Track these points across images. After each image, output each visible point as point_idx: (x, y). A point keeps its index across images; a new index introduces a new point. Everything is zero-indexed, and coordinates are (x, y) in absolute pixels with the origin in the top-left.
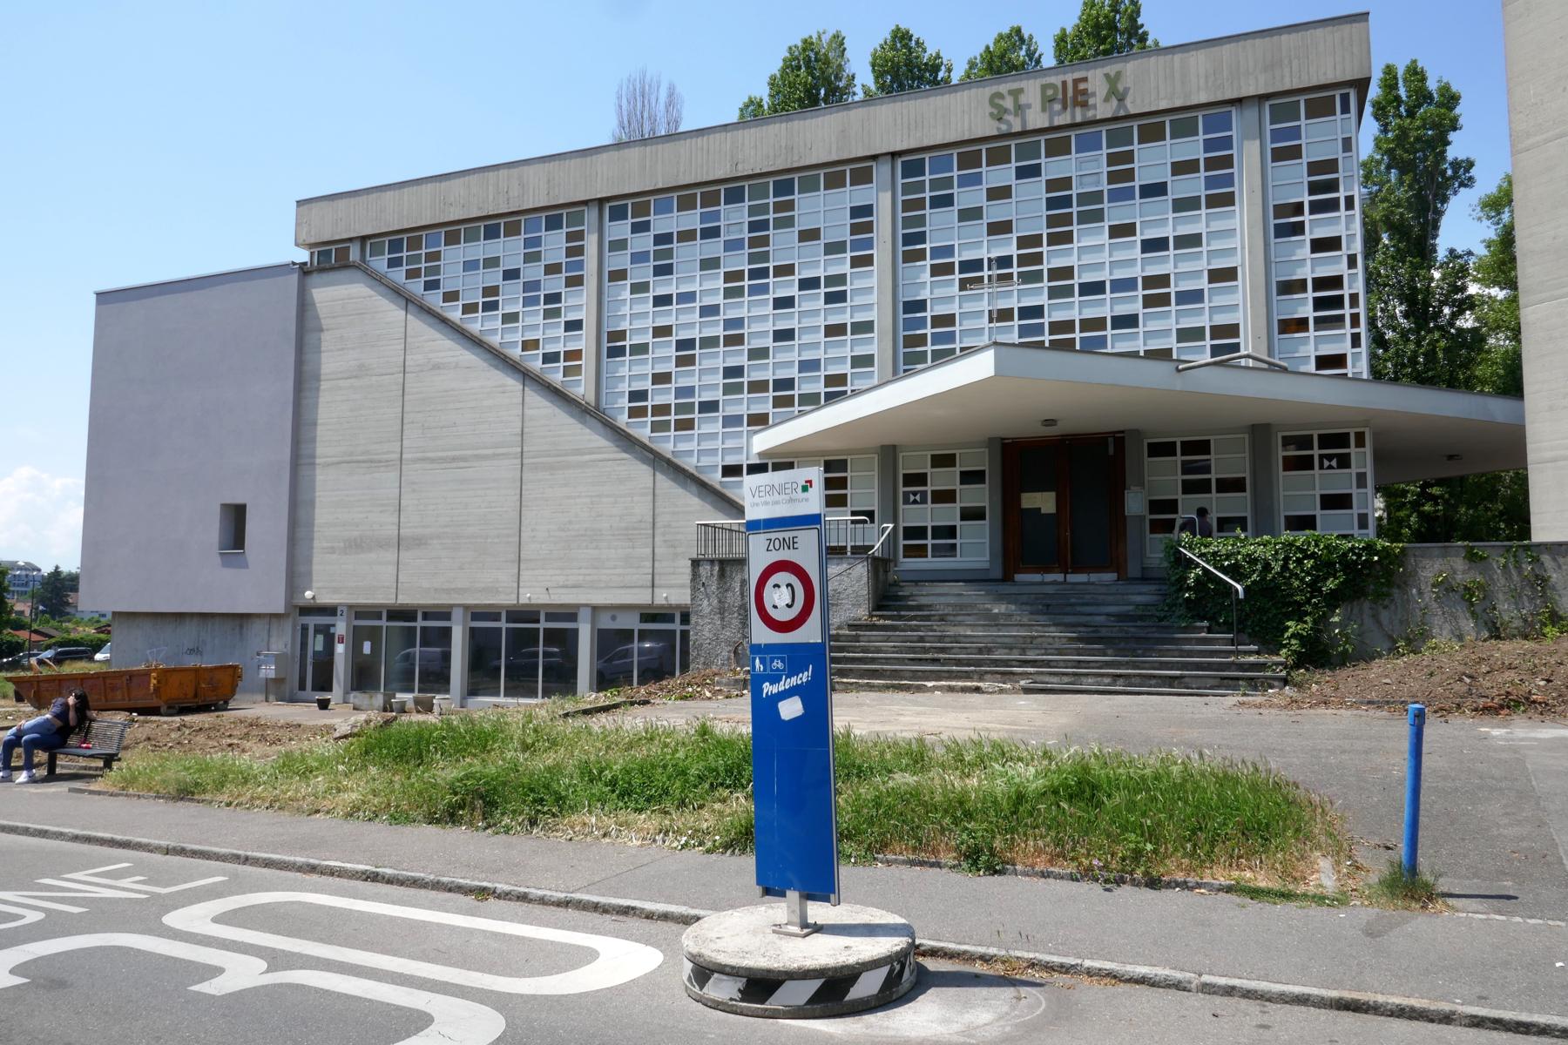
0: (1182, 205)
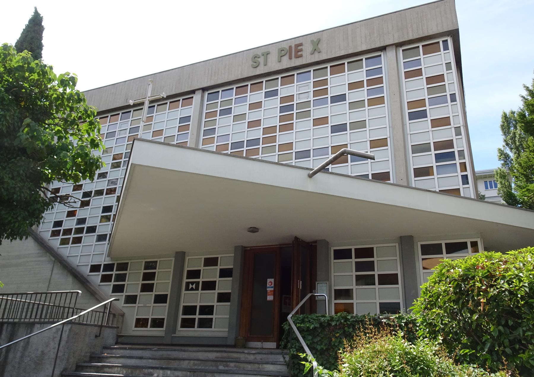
0: (353, 105)
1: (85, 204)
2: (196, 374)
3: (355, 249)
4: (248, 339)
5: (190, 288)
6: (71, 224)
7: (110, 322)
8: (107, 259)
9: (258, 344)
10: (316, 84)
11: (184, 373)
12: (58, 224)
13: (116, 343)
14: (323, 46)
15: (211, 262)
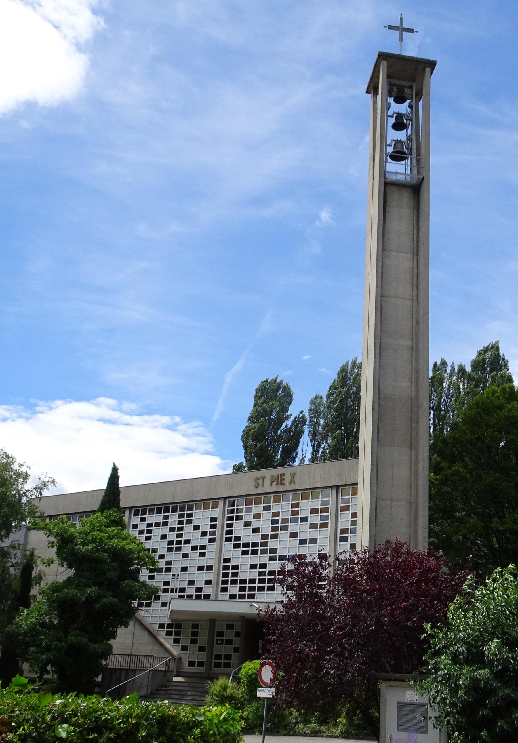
0: (313, 526)
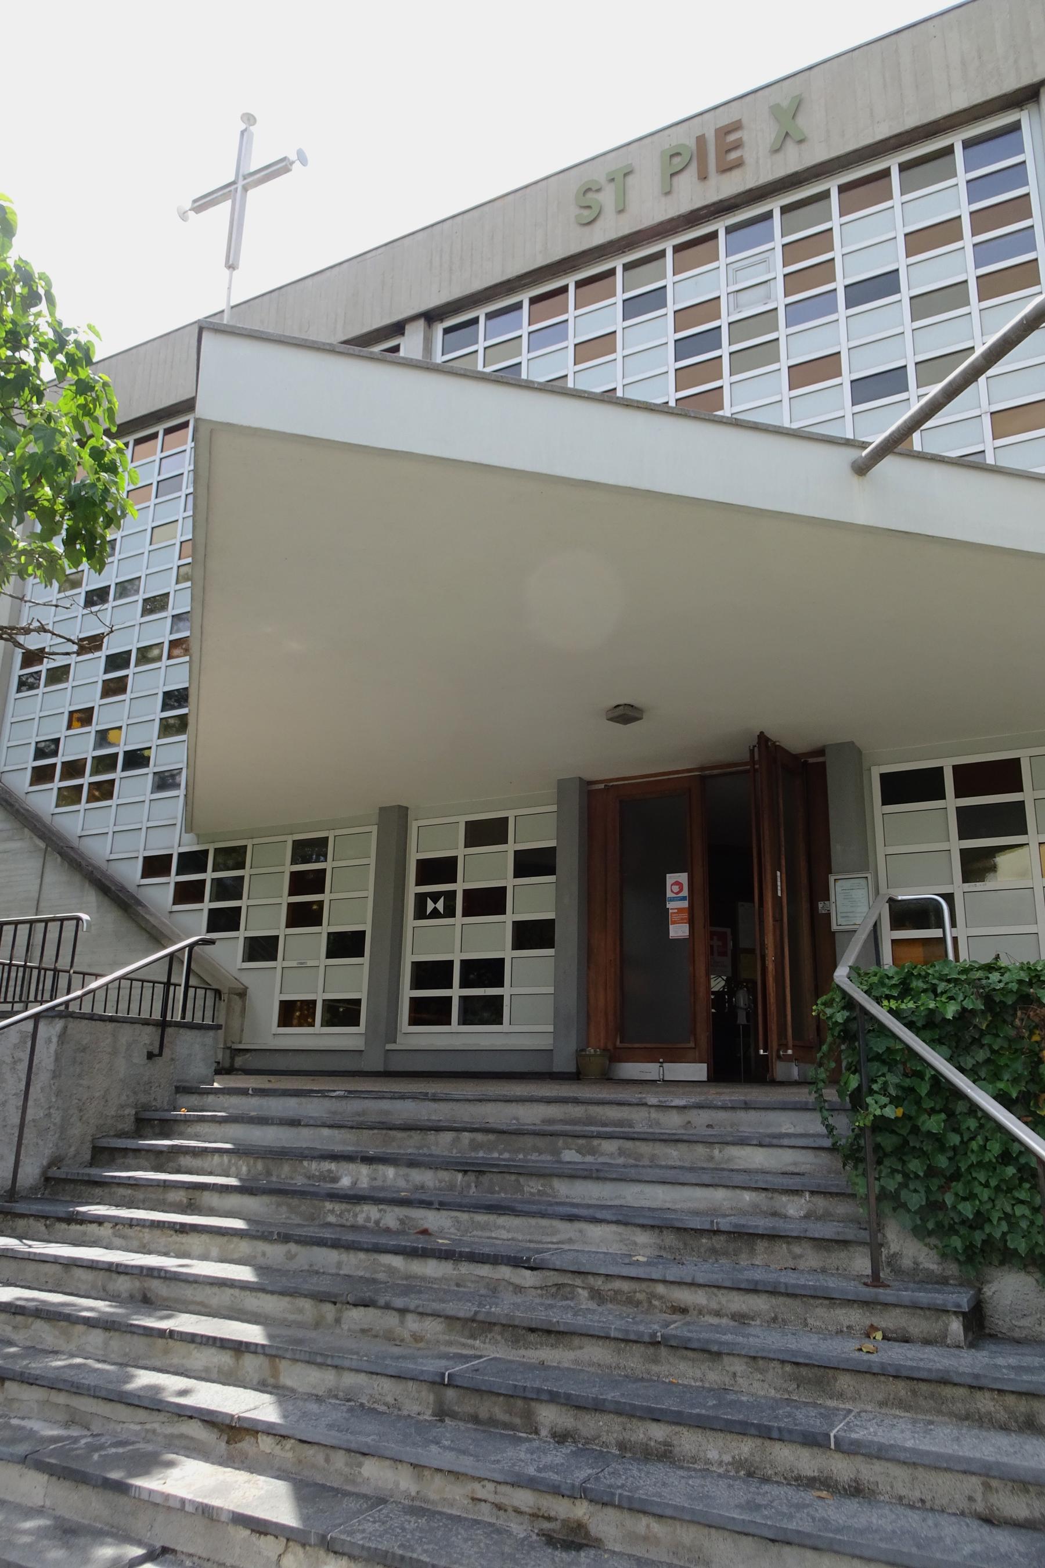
0: (925, 304)
1: (114, 688)
2: (485, 1179)
3: (955, 768)
4: (615, 1056)
5: (429, 911)
6: (79, 746)
7: (209, 1014)
8: (188, 837)
9: (649, 1070)
10: (791, 252)
11: (445, 1175)
12: (47, 749)
13: (221, 1071)
14: (812, 121)
15: (486, 832)
